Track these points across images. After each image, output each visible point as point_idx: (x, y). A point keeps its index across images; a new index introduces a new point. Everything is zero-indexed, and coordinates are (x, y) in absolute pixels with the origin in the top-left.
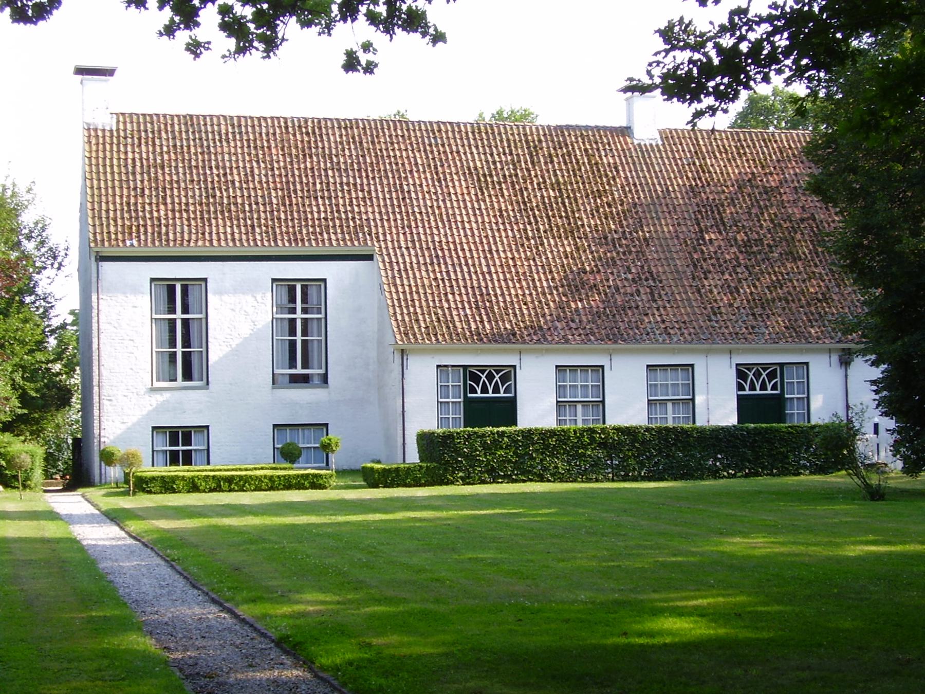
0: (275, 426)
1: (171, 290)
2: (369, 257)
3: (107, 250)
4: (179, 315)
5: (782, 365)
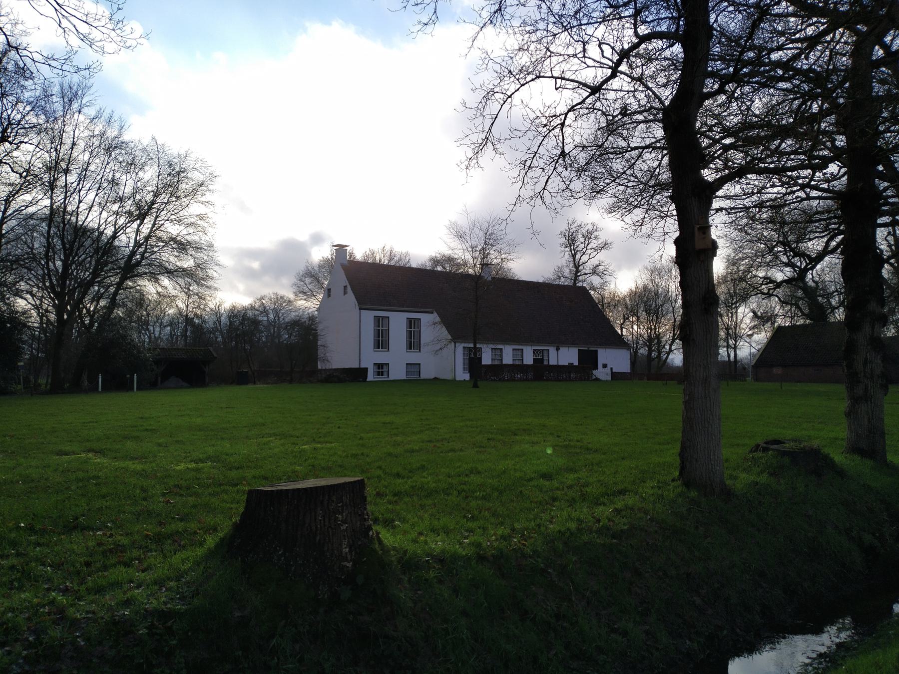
0: (407, 364)
1: (411, 322)
2: (432, 313)
3: (364, 307)
4: (381, 328)
5: (543, 350)
